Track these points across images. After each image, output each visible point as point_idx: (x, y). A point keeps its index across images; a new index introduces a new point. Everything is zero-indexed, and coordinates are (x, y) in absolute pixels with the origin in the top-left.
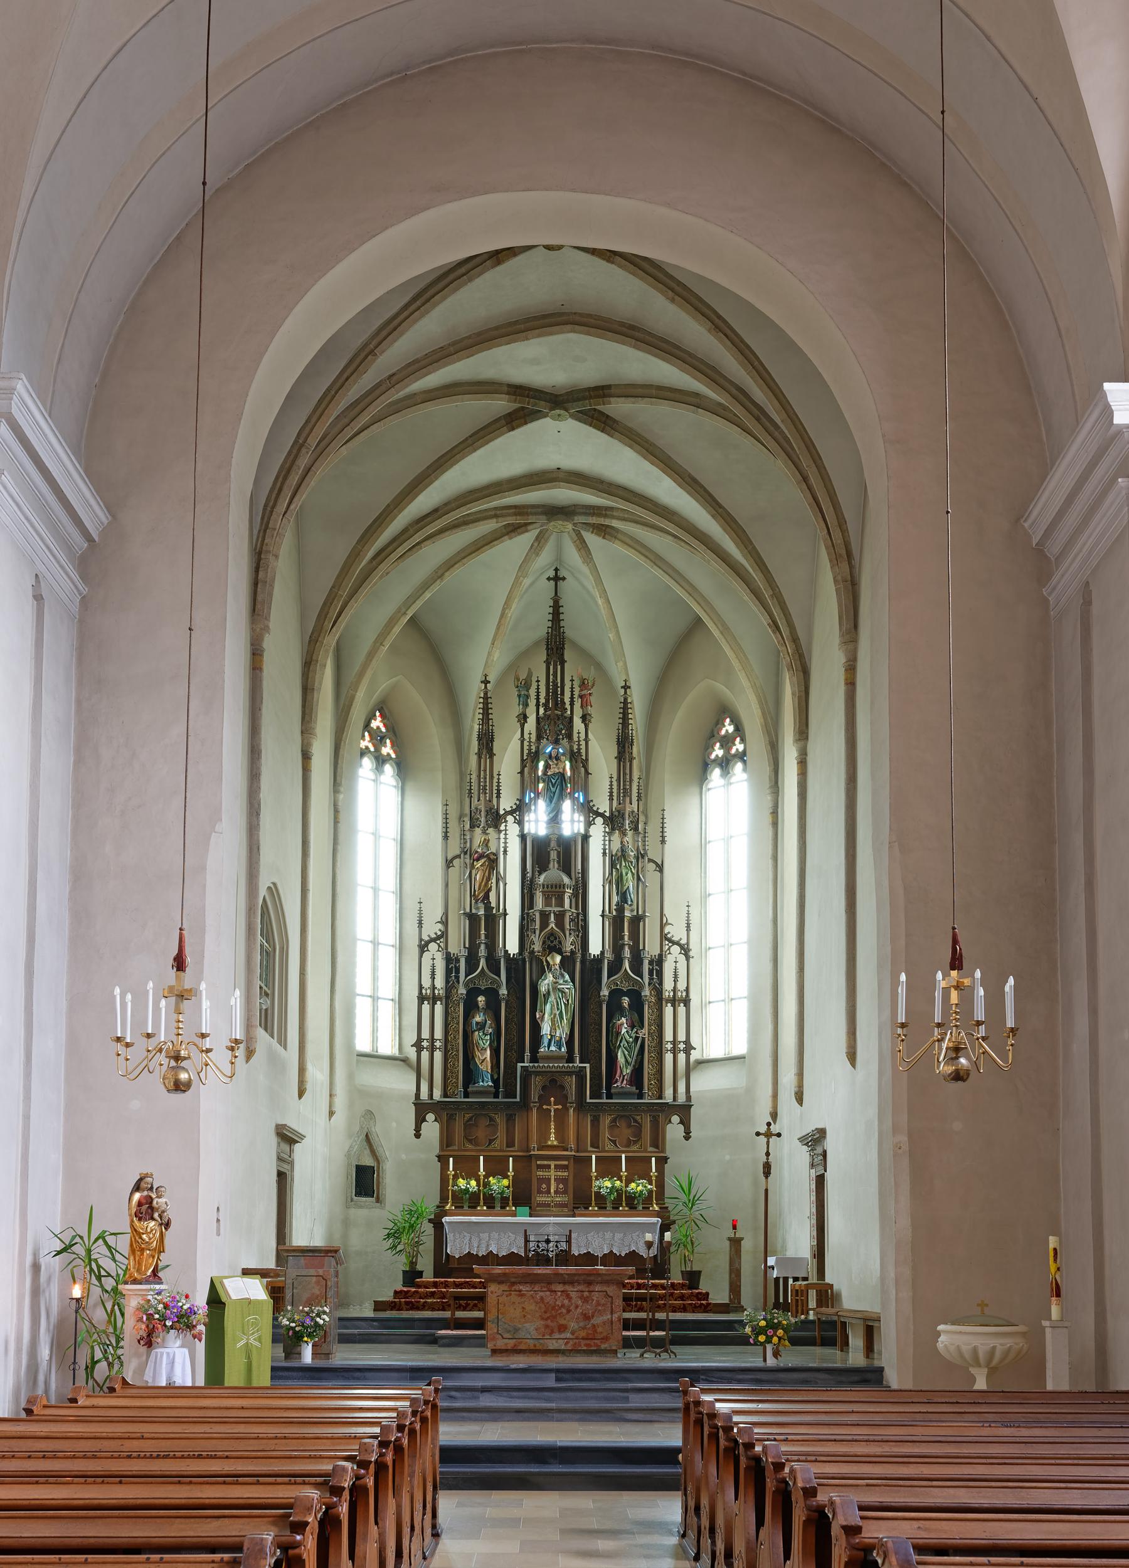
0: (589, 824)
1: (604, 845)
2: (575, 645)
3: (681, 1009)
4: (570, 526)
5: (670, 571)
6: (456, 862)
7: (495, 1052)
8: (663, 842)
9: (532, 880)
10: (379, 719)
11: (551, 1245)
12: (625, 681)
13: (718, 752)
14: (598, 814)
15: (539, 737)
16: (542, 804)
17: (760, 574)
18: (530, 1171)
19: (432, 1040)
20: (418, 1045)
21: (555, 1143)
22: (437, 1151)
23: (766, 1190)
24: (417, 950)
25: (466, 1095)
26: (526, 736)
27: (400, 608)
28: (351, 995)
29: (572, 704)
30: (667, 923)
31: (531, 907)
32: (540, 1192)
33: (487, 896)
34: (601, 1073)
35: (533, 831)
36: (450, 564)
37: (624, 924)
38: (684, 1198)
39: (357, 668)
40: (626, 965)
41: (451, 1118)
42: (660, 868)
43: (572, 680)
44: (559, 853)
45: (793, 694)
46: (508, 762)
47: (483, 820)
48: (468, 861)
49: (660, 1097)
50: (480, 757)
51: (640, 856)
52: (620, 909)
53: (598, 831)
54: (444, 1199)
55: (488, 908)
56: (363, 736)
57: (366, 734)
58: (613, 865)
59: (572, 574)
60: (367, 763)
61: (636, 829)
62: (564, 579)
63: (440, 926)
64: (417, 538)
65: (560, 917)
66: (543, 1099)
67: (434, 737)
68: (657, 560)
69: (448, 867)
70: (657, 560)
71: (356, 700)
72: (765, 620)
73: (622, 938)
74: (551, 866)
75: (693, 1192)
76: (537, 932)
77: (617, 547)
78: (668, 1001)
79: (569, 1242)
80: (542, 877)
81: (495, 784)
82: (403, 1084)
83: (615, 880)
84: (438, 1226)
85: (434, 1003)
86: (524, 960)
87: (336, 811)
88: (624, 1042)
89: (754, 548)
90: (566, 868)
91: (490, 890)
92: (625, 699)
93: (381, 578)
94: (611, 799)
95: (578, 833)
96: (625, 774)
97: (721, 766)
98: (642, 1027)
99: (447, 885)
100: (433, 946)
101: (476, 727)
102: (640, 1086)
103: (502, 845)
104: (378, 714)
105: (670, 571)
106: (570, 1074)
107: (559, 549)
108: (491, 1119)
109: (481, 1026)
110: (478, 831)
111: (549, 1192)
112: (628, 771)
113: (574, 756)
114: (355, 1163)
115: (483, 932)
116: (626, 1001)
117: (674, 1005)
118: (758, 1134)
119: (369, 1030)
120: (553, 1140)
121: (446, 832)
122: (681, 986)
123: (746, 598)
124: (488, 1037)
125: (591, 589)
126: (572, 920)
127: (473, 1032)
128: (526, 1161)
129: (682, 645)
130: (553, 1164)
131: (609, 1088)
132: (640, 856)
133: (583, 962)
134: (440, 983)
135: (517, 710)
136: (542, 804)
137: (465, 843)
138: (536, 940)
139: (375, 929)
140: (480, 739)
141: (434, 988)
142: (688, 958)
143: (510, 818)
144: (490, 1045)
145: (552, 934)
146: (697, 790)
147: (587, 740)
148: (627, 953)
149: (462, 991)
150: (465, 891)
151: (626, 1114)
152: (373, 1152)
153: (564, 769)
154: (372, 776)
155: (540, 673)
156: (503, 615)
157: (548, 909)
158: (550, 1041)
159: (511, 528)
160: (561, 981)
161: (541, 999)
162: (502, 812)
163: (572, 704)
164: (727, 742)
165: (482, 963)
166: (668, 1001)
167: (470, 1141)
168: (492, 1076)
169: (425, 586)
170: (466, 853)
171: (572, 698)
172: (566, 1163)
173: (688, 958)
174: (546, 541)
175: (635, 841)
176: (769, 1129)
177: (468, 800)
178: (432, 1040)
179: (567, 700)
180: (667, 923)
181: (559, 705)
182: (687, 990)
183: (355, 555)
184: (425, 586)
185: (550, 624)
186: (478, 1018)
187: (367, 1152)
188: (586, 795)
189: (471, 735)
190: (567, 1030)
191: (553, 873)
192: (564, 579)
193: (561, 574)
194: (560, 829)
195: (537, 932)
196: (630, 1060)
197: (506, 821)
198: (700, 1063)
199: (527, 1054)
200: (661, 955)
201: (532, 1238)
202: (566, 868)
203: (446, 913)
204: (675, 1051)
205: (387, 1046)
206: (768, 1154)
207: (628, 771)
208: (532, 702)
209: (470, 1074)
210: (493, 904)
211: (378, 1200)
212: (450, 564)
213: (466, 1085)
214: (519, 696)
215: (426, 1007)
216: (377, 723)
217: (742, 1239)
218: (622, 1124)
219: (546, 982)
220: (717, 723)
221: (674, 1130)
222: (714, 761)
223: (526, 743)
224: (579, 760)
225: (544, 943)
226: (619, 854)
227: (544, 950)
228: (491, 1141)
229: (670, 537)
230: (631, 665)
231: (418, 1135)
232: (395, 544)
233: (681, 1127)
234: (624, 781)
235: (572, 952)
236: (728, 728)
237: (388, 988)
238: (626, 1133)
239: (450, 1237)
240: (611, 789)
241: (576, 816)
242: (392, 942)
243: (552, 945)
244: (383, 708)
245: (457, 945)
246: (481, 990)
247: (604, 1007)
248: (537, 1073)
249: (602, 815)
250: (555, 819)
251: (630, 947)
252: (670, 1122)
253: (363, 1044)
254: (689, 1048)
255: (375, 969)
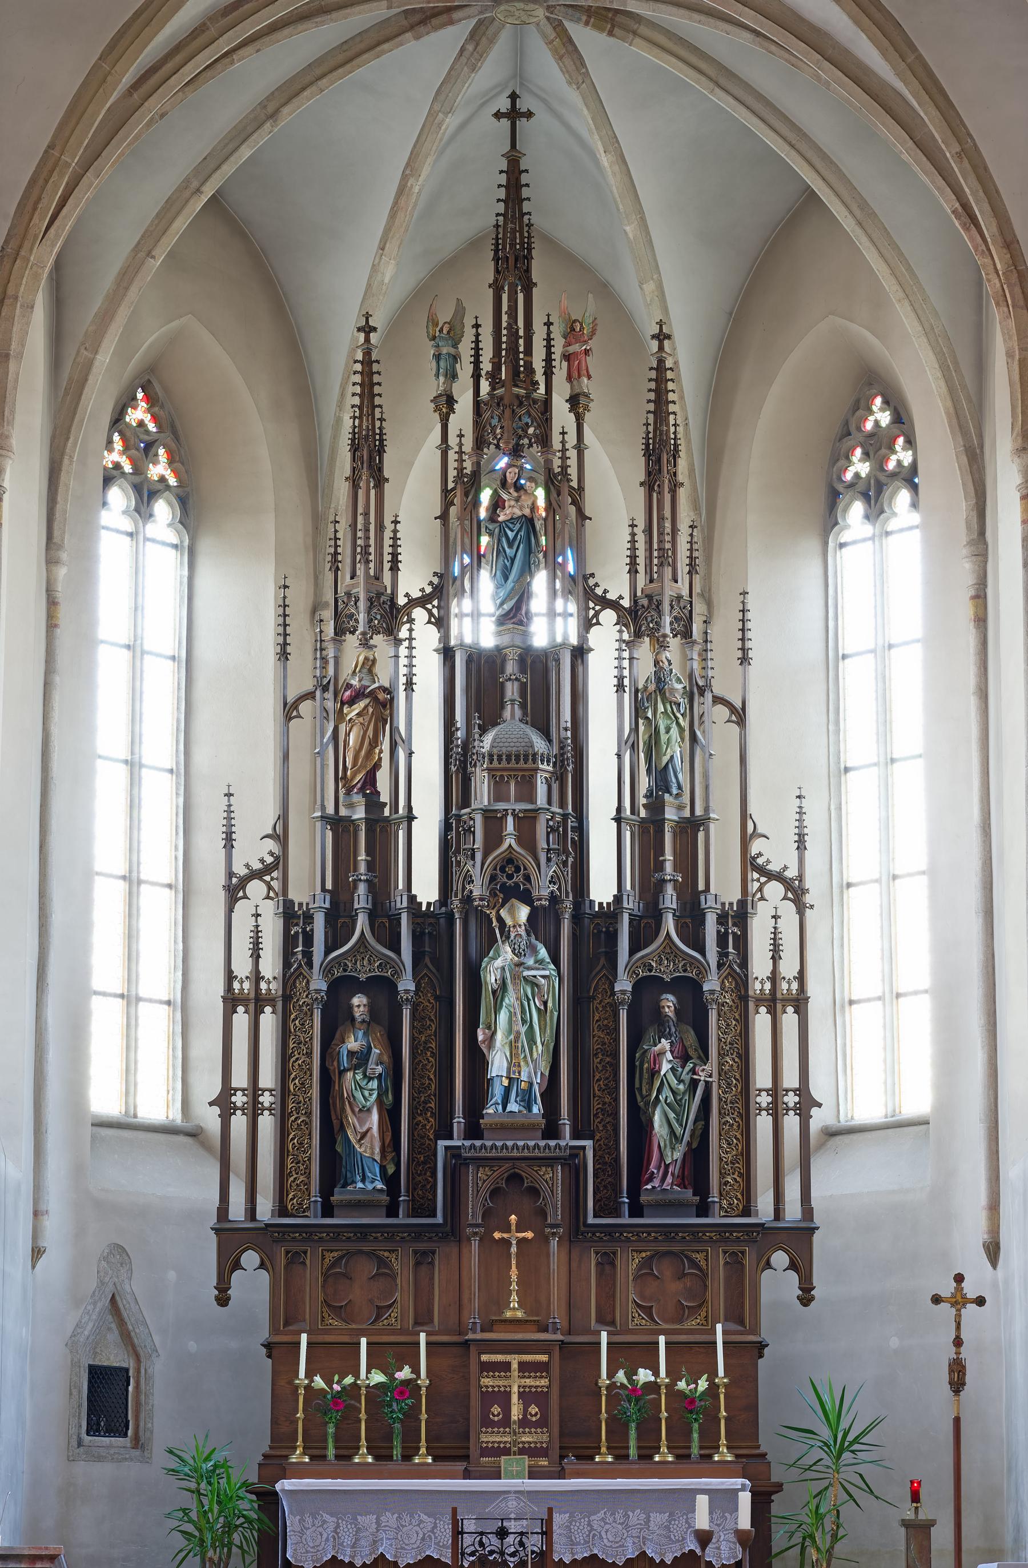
0: (588, 624)
1: (620, 668)
2: (553, 245)
3: (789, 1019)
4: (540, 12)
5: (750, 100)
6: (305, 707)
7: (391, 1116)
8: (745, 660)
9: (466, 745)
10: (143, 405)
11: (510, 1539)
12: (660, 324)
13: (859, 467)
14: (606, 603)
15: (480, 443)
16: (486, 581)
17: (934, 112)
18: (466, 1379)
19: (254, 1090)
20: (224, 1102)
21: (520, 1314)
22: (264, 1335)
23: (957, 1421)
24: (222, 895)
25: (328, 1210)
26: (453, 440)
27: (187, 181)
28: (81, 993)
29: (548, 373)
30: (756, 834)
31: (466, 803)
32: (487, 1422)
33: (370, 780)
34: (617, 1159)
35: (468, 640)
36: (292, 90)
37: (666, 834)
38: (826, 1433)
39: (97, 304)
40: (669, 924)
41: (295, 1259)
42: (739, 715)
43: (548, 324)
44: (523, 687)
45: (1009, 355)
46: (414, 493)
47: (362, 617)
48: (330, 704)
49: (747, 1212)
50: (355, 487)
51: (696, 690)
52: (656, 806)
53: (606, 637)
54: (282, 1439)
55: (373, 804)
56: (110, 442)
57: (116, 437)
58: (638, 711)
59: (544, 101)
60: (118, 497)
61: (686, 634)
62: (529, 115)
63: (271, 845)
64: (224, 45)
65: (526, 822)
66: (493, 1218)
67: (256, 444)
68: (722, 76)
69: (288, 718)
70: (722, 76)
71: (94, 370)
72: (948, 204)
73: (660, 866)
74: (507, 714)
75: (844, 1425)
76: (479, 856)
77: (639, 51)
78: (759, 1001)
79: (547, 1533)
80: (488, 739)
81: (387, 542)
82: (191, 1188)
83: (643, 743)
84: (269, 1501)
85: (258, 1011)
86: (450, 918)
87: (52, 603)
88: (666, 1092)
89: (920, 58)
90: (540, 717)
91: (377, 766)
92: (661, 362)
93: (149, 124)
94: (633, 571)
95: (564, 645)
96: (661, 518)
97: (866, 497)
98: (705, 1058)
99: (286, 757)
100: (256, 889)
101: (348, 423)
102: (701, 1187)
103: (403, 671)
104: (140, 395)
105: (750, 100)
106: (549, 1161)
107: (519, 54)
108: (382, 1263)
109: (360, 1059)
110: (352, 641)
111: (506, 1421)
112: (667, 513)
113: (554, 481)
114: (87, 1361)
115: (362, 857)
116: (669, 1003)
117: (772, 1012)
118: (937, 1300)
119: (117, 1064)
120: (514, 1310)
121: (285, 644)
122: (789, 968)
123: (905, 156)
124: (374, 1084)
125: (584, 133)
126: (551, 830)
127: (342, 1073)
128: (456, 1350)
129: (777, 248)
130: (515, 1360)
131: (634, 1191)
132: (696, 690)
133: (577, 918)
134: (270, 966)
135: (434, 386)
136: (486, 581)
137: (324, 667)
138: (476, 873)
139: (133, 847)
140: (355, 448)
141: (257, 977)
142: (801, 910)
143: (419, 614)
144: (379, 1101)
145: (510, 860)
146: (815, 544)
147: (580, 447)
148: (670, 899)
149: (319, 983)
150: (323, 766)
151: (674, 1248)
152: (127, 1337)
153: (534, 508)
154: (127, 525)
155: (480, 308)
156: (402, 190)
157: (501, 806)
158: (507, 1090)
159: (418, 17)
160: (531, 962)
161: (486, 1000)
162: (402, 601)
163: (548, 373)
164: (877, 446)
165: (362, 922)
166: (759, 1001)
167: (337, 1311)
168: (383, 1169)
169: (241, 134)
170: (325, 689)
171: (549, 360)
172: (544, 1358)
173: (801, 910)
174: (492, 41)
175: (686, 659)
176: (959, 1289)
177: (330, 576)
178: (254, 1090)
179: (538, 365)
180: (756, 834)
181: (522, 374)
182: (801, 977)
183: (96, 81)
184: (241, 134)
185: (501, 208)
186: (353, 1044)
187: (113, 1336)
188: (580, 560)
189: (335, 437)
190: (544, 1067)
191: (512, 730)
192: (529, 115)
193: (522, 105)
194: (526, 634)
195: (479, 856)
196: (679, 1130)
197: (411, 621)
198: (831, 1133)
199: (459, 1120)
200: (742, 903)
201: (469, 1526)
202: (540, 717)
203: (284, 817)
204: (776, 1111)
205: (157, 1105)
206: (958, 1342)
207: (667, 513)
208: (465, 371)
209: (336, 1164)
210: (385, 797)
211: (137, 1443)
212: (292, 90)
213: (326, 1192)
214: (438, 357)
215: (241, 1019)
216: (138, 414)
217: (932, 1523)
218: (665, 1269)
219: (498, 963)
220: (856, 407)
221: (777, 1283)
222: (851, 485)
223: (452, 456)
224: (566, 489)
225: (493, 878)
226: (652, 687)
227: (493, 893)
228: (380, 1311)
229: (747, 35)
230: (675, 290)
231: (223, 1300)
232: (178, 59)
233: (793, 1277)
234: (661, 534)
235: (554, 899)
236: (881, 417)
237: (158, 977)
238: (674, 1288)
239: (292, 1522)
240: (633, 549)
241: (559, 604)
242: (167, 877)
243: (508, 883)
244: (150, 382)
245: (306, 885)
246: (358, 981)
247: (623, 1016)
248: (481, 1162)
249: (615, 605)
250: (514, 614)
251: (678, 888)
252: (768, 1265)
253: (104, 1100)
254: (806, 1104)
255: (131, 936)
